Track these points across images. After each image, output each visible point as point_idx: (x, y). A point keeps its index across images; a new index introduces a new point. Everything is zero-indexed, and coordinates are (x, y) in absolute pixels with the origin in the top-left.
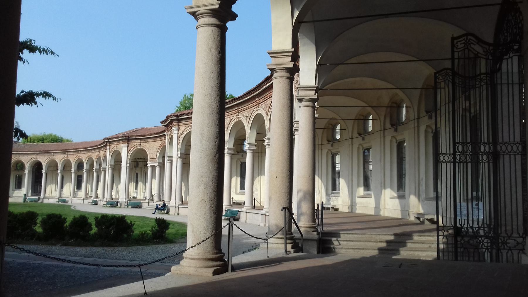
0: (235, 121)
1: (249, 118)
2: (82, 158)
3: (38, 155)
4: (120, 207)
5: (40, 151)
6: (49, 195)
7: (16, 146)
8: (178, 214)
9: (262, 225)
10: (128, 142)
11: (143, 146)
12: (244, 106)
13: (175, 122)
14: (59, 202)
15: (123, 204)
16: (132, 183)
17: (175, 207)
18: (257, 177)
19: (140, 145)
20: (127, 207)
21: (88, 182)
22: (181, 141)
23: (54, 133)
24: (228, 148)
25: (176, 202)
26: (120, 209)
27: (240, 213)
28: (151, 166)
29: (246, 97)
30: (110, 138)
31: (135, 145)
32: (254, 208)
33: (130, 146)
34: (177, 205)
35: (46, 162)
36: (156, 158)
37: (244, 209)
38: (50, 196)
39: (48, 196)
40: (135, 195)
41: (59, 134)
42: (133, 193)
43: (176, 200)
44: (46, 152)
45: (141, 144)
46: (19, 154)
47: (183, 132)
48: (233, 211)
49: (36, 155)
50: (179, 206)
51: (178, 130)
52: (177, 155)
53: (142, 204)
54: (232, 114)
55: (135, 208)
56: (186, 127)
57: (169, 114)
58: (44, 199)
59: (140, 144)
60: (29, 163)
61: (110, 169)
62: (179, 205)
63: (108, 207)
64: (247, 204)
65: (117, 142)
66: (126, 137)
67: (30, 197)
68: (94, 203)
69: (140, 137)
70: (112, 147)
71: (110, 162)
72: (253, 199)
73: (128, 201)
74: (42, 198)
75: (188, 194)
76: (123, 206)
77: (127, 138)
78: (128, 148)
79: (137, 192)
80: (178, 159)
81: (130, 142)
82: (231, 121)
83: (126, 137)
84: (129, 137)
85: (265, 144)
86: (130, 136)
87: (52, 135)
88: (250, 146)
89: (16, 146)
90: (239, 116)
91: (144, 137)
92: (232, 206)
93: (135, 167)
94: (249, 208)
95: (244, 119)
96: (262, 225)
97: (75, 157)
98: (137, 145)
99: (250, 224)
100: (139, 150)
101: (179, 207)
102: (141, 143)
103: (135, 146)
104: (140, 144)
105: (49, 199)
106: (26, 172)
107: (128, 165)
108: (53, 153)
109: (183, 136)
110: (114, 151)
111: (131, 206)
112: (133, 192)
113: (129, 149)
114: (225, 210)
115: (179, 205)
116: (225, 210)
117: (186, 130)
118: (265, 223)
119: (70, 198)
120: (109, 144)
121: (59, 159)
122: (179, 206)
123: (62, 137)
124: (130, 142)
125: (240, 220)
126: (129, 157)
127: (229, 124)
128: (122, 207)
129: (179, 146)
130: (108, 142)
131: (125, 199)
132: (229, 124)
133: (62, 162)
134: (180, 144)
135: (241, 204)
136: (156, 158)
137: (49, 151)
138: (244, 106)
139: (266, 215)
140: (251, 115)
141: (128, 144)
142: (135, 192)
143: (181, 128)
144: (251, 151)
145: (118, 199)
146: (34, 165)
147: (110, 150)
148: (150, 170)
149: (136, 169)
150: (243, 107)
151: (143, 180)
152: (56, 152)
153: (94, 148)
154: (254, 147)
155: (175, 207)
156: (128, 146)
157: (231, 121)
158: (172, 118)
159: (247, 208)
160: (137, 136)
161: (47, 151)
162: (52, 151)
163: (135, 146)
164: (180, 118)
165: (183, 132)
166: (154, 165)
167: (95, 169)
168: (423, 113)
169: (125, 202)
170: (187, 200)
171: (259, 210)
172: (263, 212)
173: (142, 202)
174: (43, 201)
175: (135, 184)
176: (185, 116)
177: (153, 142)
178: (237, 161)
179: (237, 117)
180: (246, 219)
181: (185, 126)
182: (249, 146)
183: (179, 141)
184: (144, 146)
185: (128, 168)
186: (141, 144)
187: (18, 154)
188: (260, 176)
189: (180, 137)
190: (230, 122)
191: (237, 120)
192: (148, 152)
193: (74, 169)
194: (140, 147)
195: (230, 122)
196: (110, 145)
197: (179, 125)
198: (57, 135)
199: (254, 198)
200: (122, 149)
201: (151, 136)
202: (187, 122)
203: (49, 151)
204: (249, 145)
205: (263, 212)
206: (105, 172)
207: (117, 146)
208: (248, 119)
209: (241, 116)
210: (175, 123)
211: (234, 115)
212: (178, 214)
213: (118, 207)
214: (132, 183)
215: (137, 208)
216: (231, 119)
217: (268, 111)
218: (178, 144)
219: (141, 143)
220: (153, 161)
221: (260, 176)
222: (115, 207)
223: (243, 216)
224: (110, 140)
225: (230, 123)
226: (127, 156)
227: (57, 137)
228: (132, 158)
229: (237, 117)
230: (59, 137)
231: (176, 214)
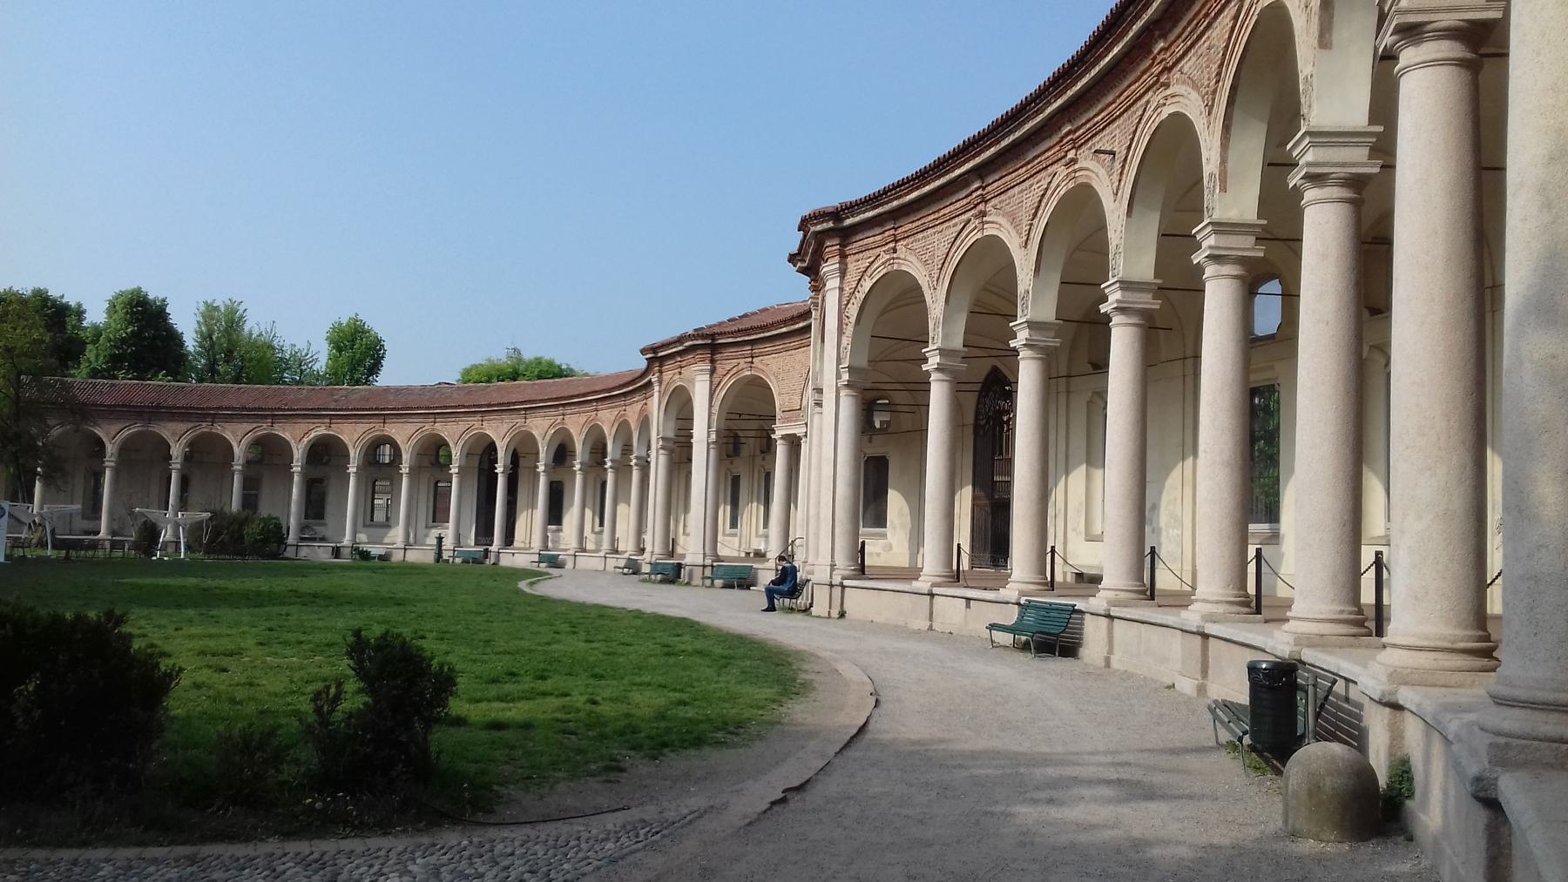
0: (1062, 193)
1: (1120, 157)
2: (603, 422)
3: (484, 418)
4: (688, 584)
5: (489, 405)
6: (523, 542)
7: (429, 392)
8: (842, 615)
9: (1187, 686)
10: (713, 354)
11: (760, 366)
12: (1100, 107)
13: (828, 244)
14: (541, 565)
15: (698, 572)
16: (755, 504)
17: (831, 586)
18: (1175, 465)
19: (749, 365)
20: (708, 582)
21: (673, 511)
22: (853, 319)
23: (547, 355)
24: (1031, 325)
25: (704, 554)
26: (687, 589)
27: (1082, 619)
28: (784, 437)
29: (1108, 50)
30: (659, 347)
31: (734, 367)
32: (1258, 611)
33: (720, 370)
34: (837, 580)
35: (507, 440)
36: (800, 409)
37: (1098, 602)
38: (528, 546)
39: (522, 545)
40: (762, 548)
41: (562, 359)
42: (758, 539)
43: (833, 557)
44: (505, 408)
45: (755, 360)
46: (433, 416)
47: (860, 279)
48: (1049, 608)
49: (478, 417)
50: (846, 583)
51: (843, 273)
52: (838, 376)
53: (756, 574)
54: (1047, 167)
55: (734, 588)
56: (872, 259)
57: (806, 213)
58: (501, 555)
59: (750, 359)
60: (461, 443)
61: (661, 451)
62: (712, 562)
63: (654, 582)
64: (1116, 577)
65: (679, 359)
66: (703, 337)
67: (471, 547)
68: (659, 577)
69: (748, 335)
70: (667, 376)
71: (661, 429)
72: (1145, 558)
73: (715, 564)
74: (403, 546)
75: (921, 544)
76: (697, 580)
77: (710, 341)
78: (711, 375)
79: (766, 536)
80: (843, 393)
81: (718, 357)
82: (1043, 195)
83: (703, 337)
84: (713, 336)
85: (1197, 258)
86: (718, 334)
87: (544, 362)
88: (1128, 294)
89: (429, 392)
90: (1076, 166)
91: (762, 335)
92: (1052, 585)
93: (762, 452)
94: (1123, 595)
95: (1102, 172)
96: (1187, 686)
97: (585, 420)
98: (740, 367)
99: (1127, 676)
100: (746, 384)
101: (843, 587)
102: (753, 357)
103: (735, 370)
104: (750, 359)
105: (513, 554)
106: (453, 471)
107: (713, 436)
108: (525, 409)
109: (861, 296)
110: (672, 389)
111: (721, 581)
112: (757, 536)
113: (716, 380)
114: (1018, 604)
115: (606, 553)
116: (1018, 604)
117: (870, 271)
118: (1199, 676)
119: (568, 552)
120: (657, 368)
121: (541, 428)
122: (846, 583)
123: (571, 367)
124: (720, 355)
125: (1083, 652)
126: (716, 409)
127: (1035, 215)
128: (694, 583)
129: (846, 341)
130: (657, 356)
131: (702, 556)
132: (1035, 215)
133: (548, 437)
134: (849, 330)
135: (1088, 581)
136: (800, 409)
137: (514, 404)
138: (1100, 107)
139: (1205, 636)
140: (1132, 139)
141: (713, 361)
142: (760, 536)
143: (851, 267)
144: (1134, 320)
145: (683, 556)
146: (484, 450)
147: (663, 387)
148: (781, 450)
149: (764, 459)
150: (1095, 114)
151: (759, 492)
152: (530, 407)
153: (631, 388)
154: (1146, 301)
155: (831, 586)
156: (713, 371)
157: (1043, 195)
158: (819, 228)
159: (1111, 595)
160: (739, 331)
161: (509, 404)
162: (522, 403)
163: (735, 370)
164: (848, 222)
165: (860, 279)
166: (795, 435)
167: (637, 458)
168: (1296, 636)
169: (704, 566)
170: (920, 566)
171: (1174, 609)
172: (1191, 617)
173: (755, 566)
174: (499, 561)
175: (762, 508)
176: (864, 212)
177: (790, 353)
178: (1090, 402)
179: (1070, 170)
180: (1111, 651)
181: (867, 254)
182: (1123, 296)
183: (846, 321)
184: (764, 368)
185: (712, 446)
186: (752, 363)
187: (430, 416)
188: (1189, 461)
189: (848, 302)
190: (1040, 201)
191: (1071, 185)
192: (776, 386)
193: (582, 459)
194: (749, 373)
195: (1040, 201)
196: (661, 372)
197: (846, 256)
198: (557, 362)
199: (1148, 551)
200: (692, 381)
201: (784, 330)
202: (871, 239)
203: (514, 404)
204: (1121, 289)
205: (1191, 617)
206: (645, 466)
207: (680, 373)
208: (1118, 165)
209: (1086, 160)
210: (832, 246)
211: (1055, 166)
212: (842, 615)
213: (681, 584)
214: (755, 504)
215: (741, 587)
216: (1045, 186)
217: (1217, 82)
218: (840, 332)
219: (753, 357)
220: (791, 421)
221: (1191, 458)
222: (672, 582)
223: (1093, 633)
224: (660, 354)
225: (1038, 207)
226: (710, 406)
227: (555, 367)
228: (724, 414)
229: (1070, 170)
230: (564, 367)
231: (835, 613)
